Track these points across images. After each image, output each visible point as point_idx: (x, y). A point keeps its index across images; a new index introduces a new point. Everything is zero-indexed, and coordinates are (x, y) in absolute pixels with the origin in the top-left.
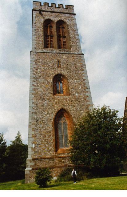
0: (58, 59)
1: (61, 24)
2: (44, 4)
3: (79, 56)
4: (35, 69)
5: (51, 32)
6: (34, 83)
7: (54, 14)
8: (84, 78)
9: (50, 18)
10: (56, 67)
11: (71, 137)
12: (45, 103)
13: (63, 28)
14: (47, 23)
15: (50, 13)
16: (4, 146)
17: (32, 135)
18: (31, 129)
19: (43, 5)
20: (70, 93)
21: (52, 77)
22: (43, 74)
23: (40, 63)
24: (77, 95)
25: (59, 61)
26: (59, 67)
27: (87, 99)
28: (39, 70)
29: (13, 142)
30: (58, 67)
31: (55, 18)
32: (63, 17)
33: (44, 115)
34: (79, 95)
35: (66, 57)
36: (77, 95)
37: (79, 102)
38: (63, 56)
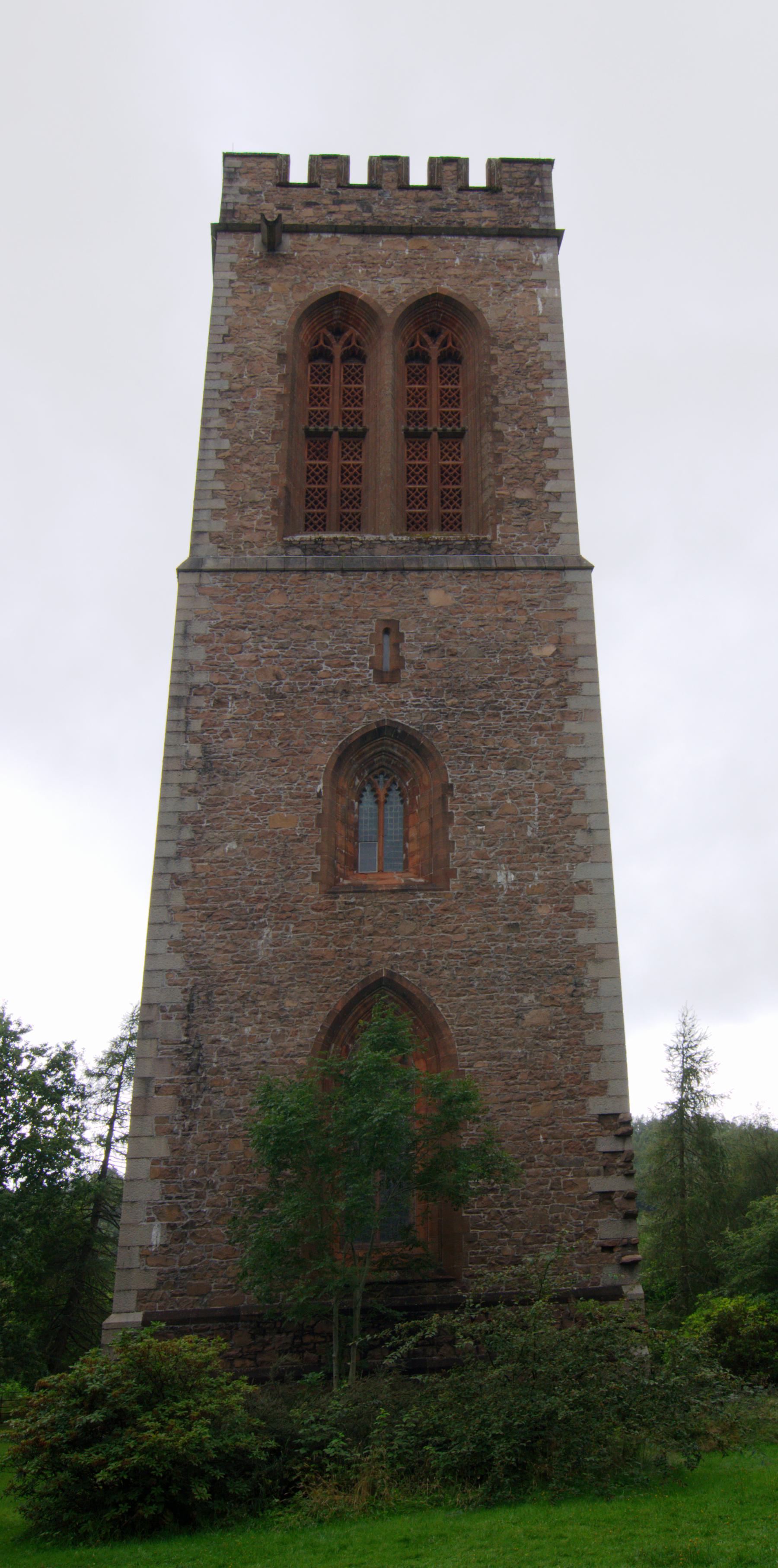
0: (387, 612)
1: (439, 327)
2: (431, 177)
3: (552, 580)
4: (200, 702)
5: (354, 398)
6: (191, 804)
7: (382, 245)
8: (573, 752)
9: (346, 285)
10: (359, 682)
11: (157, 1212)
12: (263, 944)
13: (451, 357)
14: (333, 328)
15: (353, 241)
16: (619, 1124)
17: (156, 1162)
18: (150, 1121)
19: (305, 180)
20: (453, 864)
21: (323, 755)
22: (259, 734)
23: (247, 656)
24: (503, 877)
25: (389, 628)
26: (388, 677)
27: (581, 903)
28: (232, 707)
29: (674, 1106)
30: (380, 676)
31: (386, 280)
32: (453, 268)
33: (247, 1030)
34: (520, 879)
35: (449, 600)
36: (503, 877)
37: (514, 927)
38: (425, 587)
